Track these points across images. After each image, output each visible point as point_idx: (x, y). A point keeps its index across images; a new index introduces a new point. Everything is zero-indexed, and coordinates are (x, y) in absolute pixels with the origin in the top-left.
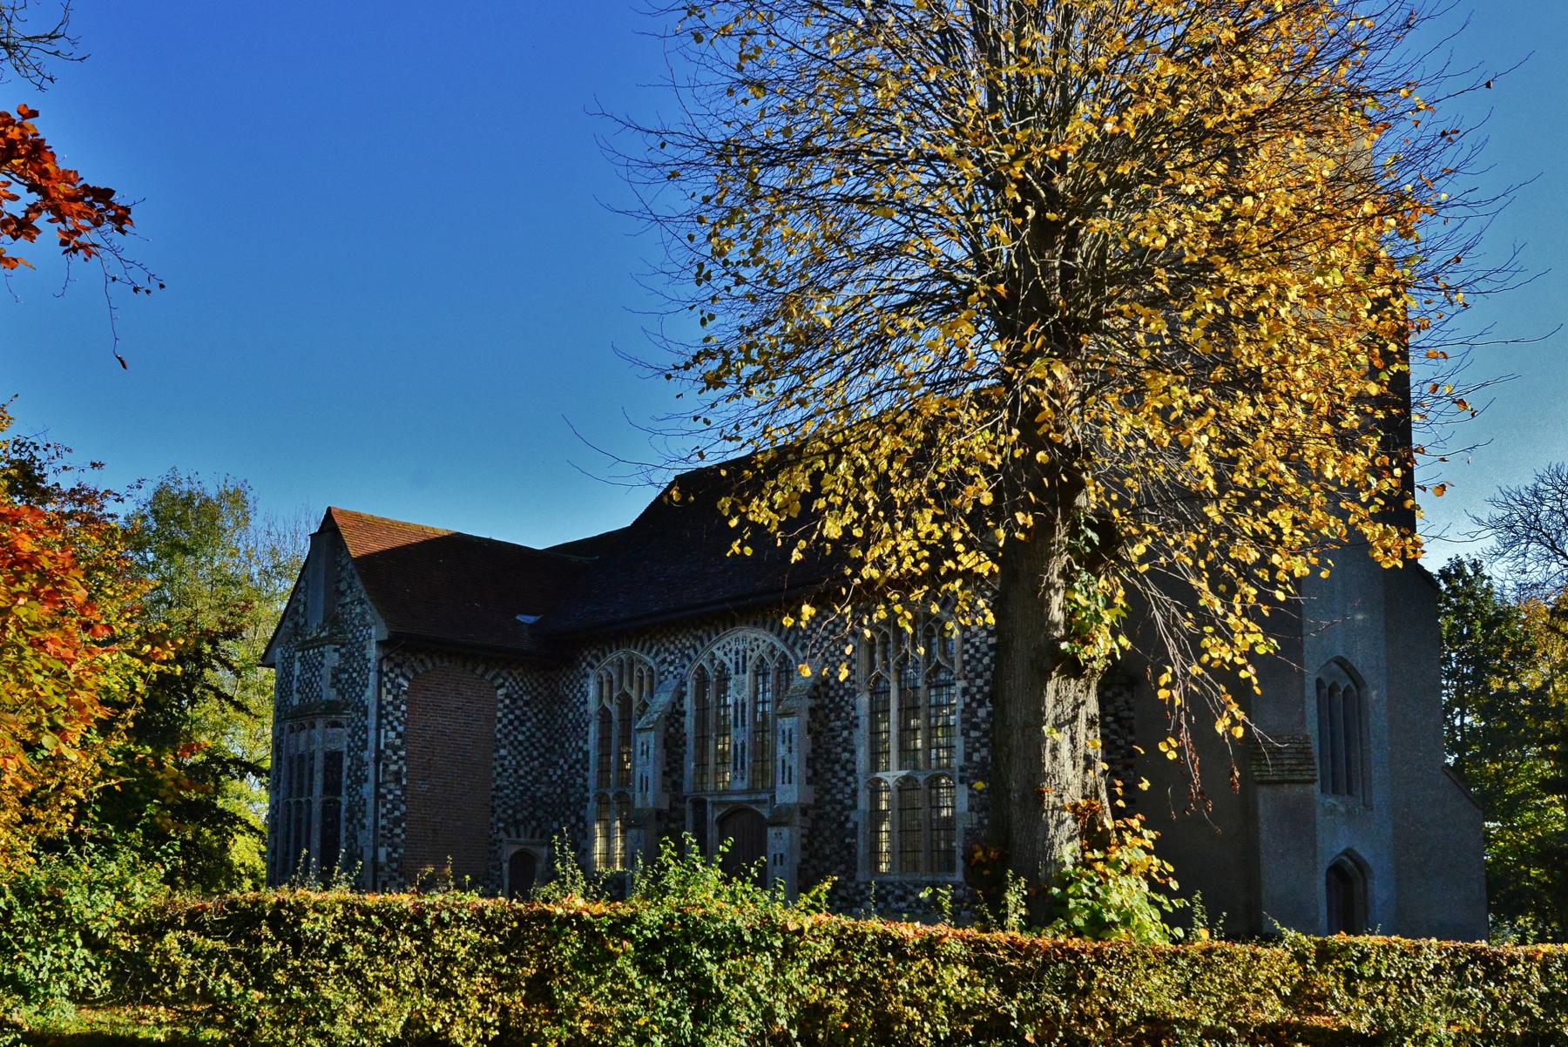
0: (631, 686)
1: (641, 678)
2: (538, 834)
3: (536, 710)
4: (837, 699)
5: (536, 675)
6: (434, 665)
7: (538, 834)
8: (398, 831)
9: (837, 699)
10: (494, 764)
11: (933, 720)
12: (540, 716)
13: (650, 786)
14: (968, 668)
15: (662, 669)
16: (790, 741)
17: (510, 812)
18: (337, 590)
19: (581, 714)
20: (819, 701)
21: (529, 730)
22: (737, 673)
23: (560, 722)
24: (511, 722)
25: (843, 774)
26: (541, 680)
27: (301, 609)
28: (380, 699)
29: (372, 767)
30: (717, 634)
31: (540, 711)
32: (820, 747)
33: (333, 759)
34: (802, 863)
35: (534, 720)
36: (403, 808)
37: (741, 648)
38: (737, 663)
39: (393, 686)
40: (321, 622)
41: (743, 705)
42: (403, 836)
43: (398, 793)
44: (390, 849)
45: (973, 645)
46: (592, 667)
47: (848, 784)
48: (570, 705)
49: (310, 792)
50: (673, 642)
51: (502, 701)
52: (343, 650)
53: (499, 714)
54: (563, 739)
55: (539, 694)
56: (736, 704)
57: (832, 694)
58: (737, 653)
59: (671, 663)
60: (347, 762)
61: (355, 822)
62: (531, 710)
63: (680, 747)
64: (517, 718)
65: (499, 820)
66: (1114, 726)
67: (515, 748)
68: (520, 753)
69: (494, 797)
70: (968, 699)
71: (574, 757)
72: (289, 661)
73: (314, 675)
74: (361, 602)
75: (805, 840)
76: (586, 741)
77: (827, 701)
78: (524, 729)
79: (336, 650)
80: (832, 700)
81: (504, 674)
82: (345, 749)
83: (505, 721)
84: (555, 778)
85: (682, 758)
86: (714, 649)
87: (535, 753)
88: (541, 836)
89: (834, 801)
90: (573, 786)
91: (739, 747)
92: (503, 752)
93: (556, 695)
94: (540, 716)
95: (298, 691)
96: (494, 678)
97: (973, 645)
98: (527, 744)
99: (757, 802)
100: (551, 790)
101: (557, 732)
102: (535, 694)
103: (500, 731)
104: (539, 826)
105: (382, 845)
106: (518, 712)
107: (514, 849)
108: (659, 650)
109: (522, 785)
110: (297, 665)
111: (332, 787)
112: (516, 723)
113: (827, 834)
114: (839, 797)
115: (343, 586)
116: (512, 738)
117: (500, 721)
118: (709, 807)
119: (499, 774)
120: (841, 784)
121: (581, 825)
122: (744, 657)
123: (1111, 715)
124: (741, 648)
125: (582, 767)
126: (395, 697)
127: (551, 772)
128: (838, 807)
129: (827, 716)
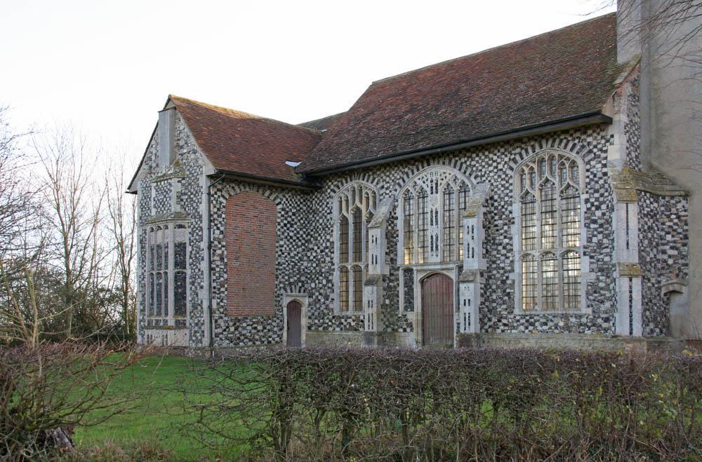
0: (361, 202)
1: (368, 198)
2: (302, 291)
3: (299, 218)
4: (500, 207)
5: (299, 197)
6: (241, 190)
7: (302, 291)
8: (222, 289)
9: (500, 207)
10: (277, 250)
11: (524, 223)
12: (302, 222)
13: (379, 261)
14: (589, 187)
15: (381, 192)
16: (473, 233)
17: (286, 278)
18: (178, 145)
19: (328, 220)
20: (488, 208)
21: (295, 229)
22: (432, 193)
23: (314, 224)
24: (285, 225)
25: (504, 252)
26: (302, 200)
27: (153, 158)
28: (210, 211)
29: (206, 252)
30: (423, 167)
31: (302, 219)
32: (489, 236)
33: (180, 248)
34: (481, 305)
35: (298, 224)
36: (225, 276)
37: (434, 178)
38: (432, 187)
39: (217, 203)
40: (168, 164)
41: (437, 213)
42: (226, 293)
43: (222, 267)
44: (219, 301)
45: (592, 173)
46: (335, 192)
47: (508, 258)
48: (320, 215)
49: (167, 267)
50: (388, 176)
51: (280, 213)
52: (183, 182)
53: (279, 220)
54: (317, 235)
55: (301, 208)
56: (432, 212)
57: (496, 204)
58: (432, 181)
59: (387, 189)
60: (189, 249)
61: (196, 284)
62: (297, 218)
63: (395, 238)
64: (289, 222)
65: (280, 282)
66: (676, 221)
67: (288, 240)
68: (292, 243)
69: (277, 269)
70: (589, 205)
71: (324, 245)
72: (147, 188)
73: (165, 196)
74: (195, 152)
75: (482, 291)
76: (331, 236)
77: (493, 209)
78: (293, 229)
79: (179, 182)
80: (496, 208)
81: (281, 196)
82: (188, 242)
83: (282, 224)
84: (311, 258)
85: (396, 245)
86: (416, 179)
87: (300, 243)
88: (304, 292)
89: (498, 268)
90: (324, 262)
91: (434, 237)
92: (282, 243)
93: (311, 209)
94: (302, 222)
95: (155, 207)
96: (275, 199)
97: (592, 173)
98: (294, 238)
99: (448, 269)
100: (309, 265)
101: (312, 231)
102: (298, 208)
103: (279, 230)
104: (303, 286)
105: (214, 298)
106: (289, 219)
107: (290, 299)
108: (379, 180)
109: (293, 262)
110: (153, 192)
111: (180, 264)
112: (288, 225)
113: (494, 287)
114: (502, 265)
115: (181, 143)
116: (286, 234)
117: (279, 224)
118: (415, 272)
119: (280, 256)
120: (503, 258)
121: (330, 285)
122: (437, 184)
123: (675, 214)
124: (434, 178)
125: (330, 251)
126: (218, 209)
127: (309, 254)
128: (502, 271)
129: (493, 218)
